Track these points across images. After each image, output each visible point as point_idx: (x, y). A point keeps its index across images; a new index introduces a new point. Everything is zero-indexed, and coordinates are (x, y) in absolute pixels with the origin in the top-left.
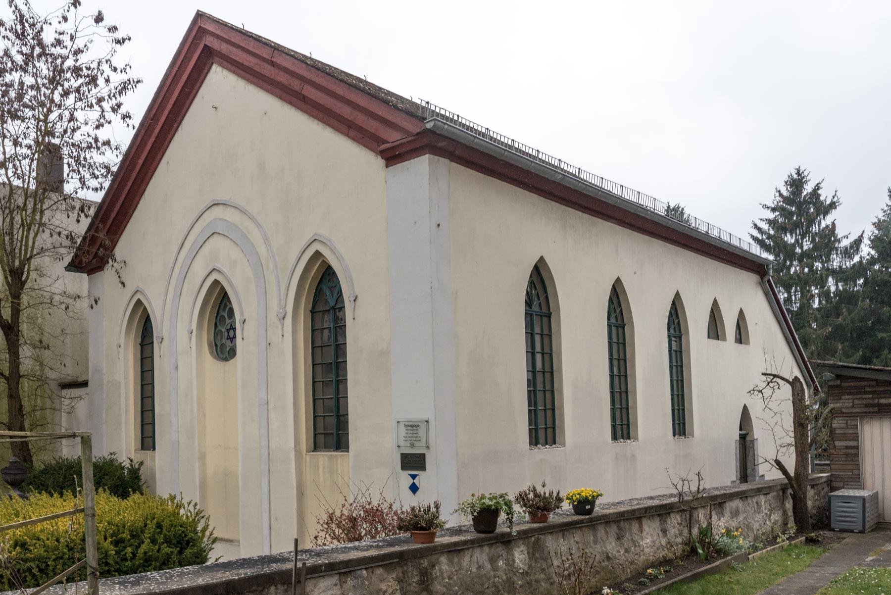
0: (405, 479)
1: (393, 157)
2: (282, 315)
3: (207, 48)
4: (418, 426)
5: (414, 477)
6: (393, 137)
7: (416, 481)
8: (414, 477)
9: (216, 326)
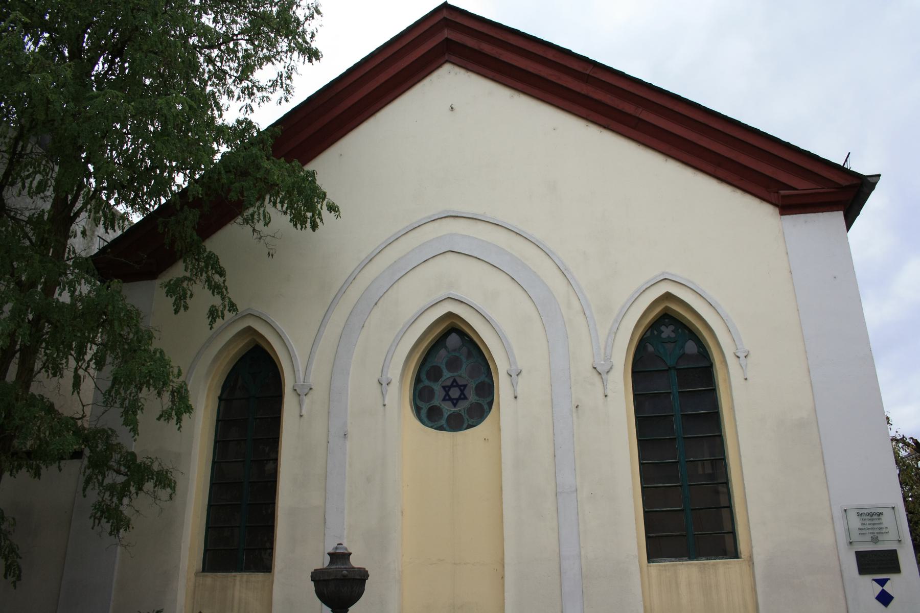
0: (868, 586)
1: (790, 205)
2: (607, 368)
3: (447, 41)
4: (881, 514)
5: (882, 582)
6: (803, 186)
7: (887, 588)
8: (882, 582)
9: (418, 380)
